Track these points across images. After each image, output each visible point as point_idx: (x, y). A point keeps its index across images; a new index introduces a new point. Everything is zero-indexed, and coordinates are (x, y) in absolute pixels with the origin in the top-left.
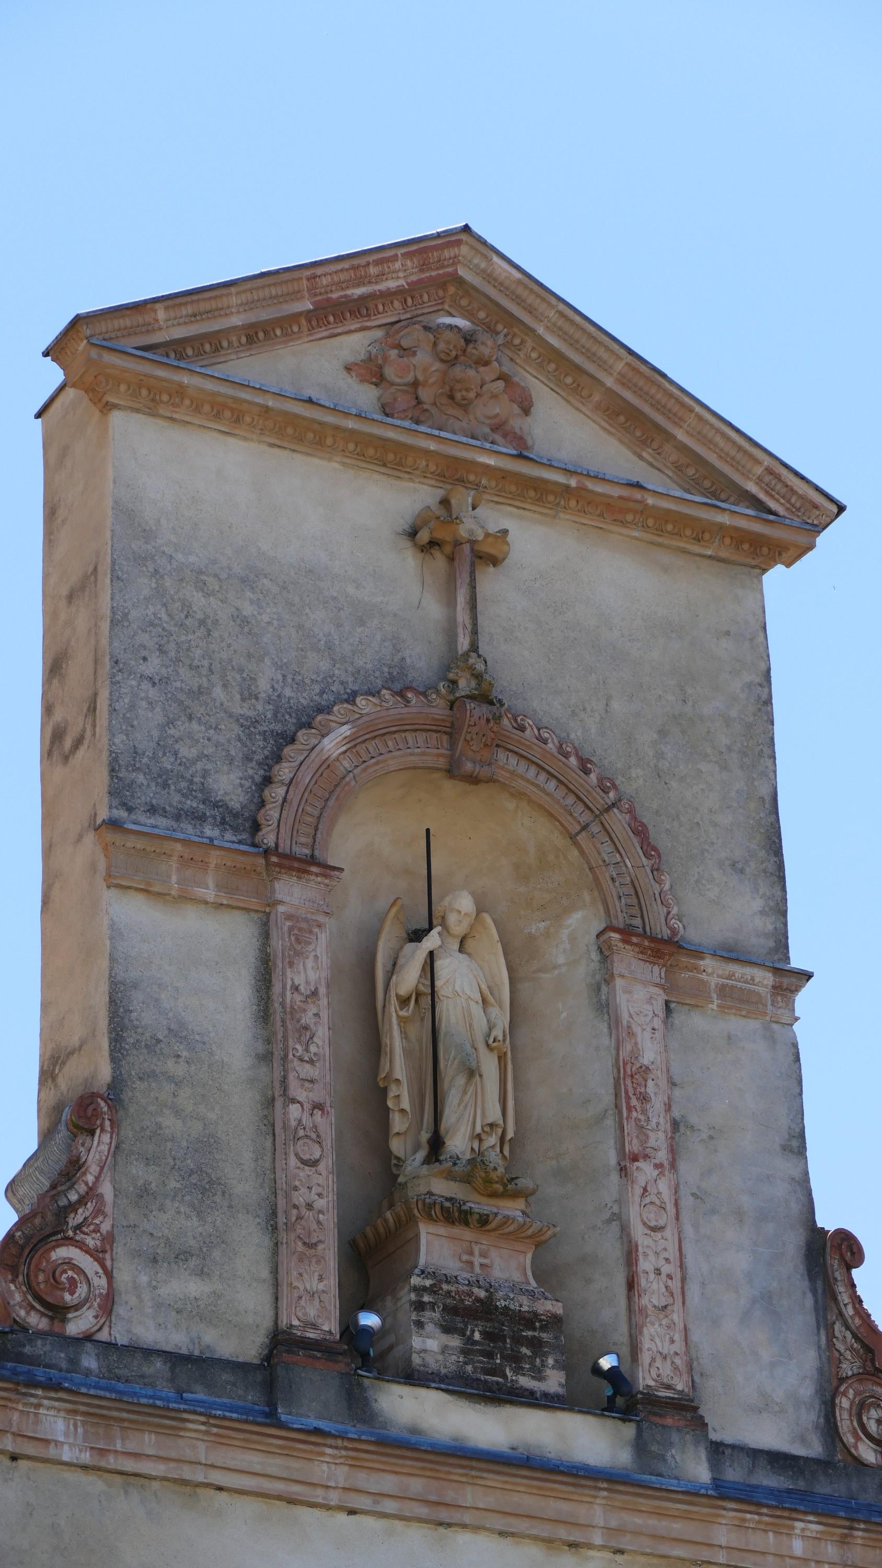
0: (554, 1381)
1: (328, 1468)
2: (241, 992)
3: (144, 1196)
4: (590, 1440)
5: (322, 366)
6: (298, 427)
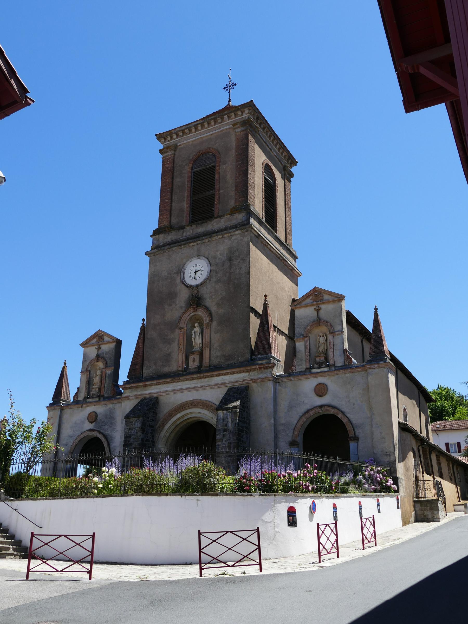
0: (324, 366)
1: (309, 376)
2: (304, 347)
3: (298, 362)
4: (326, 369)
5: (309, 300)
6: (306, 306)
